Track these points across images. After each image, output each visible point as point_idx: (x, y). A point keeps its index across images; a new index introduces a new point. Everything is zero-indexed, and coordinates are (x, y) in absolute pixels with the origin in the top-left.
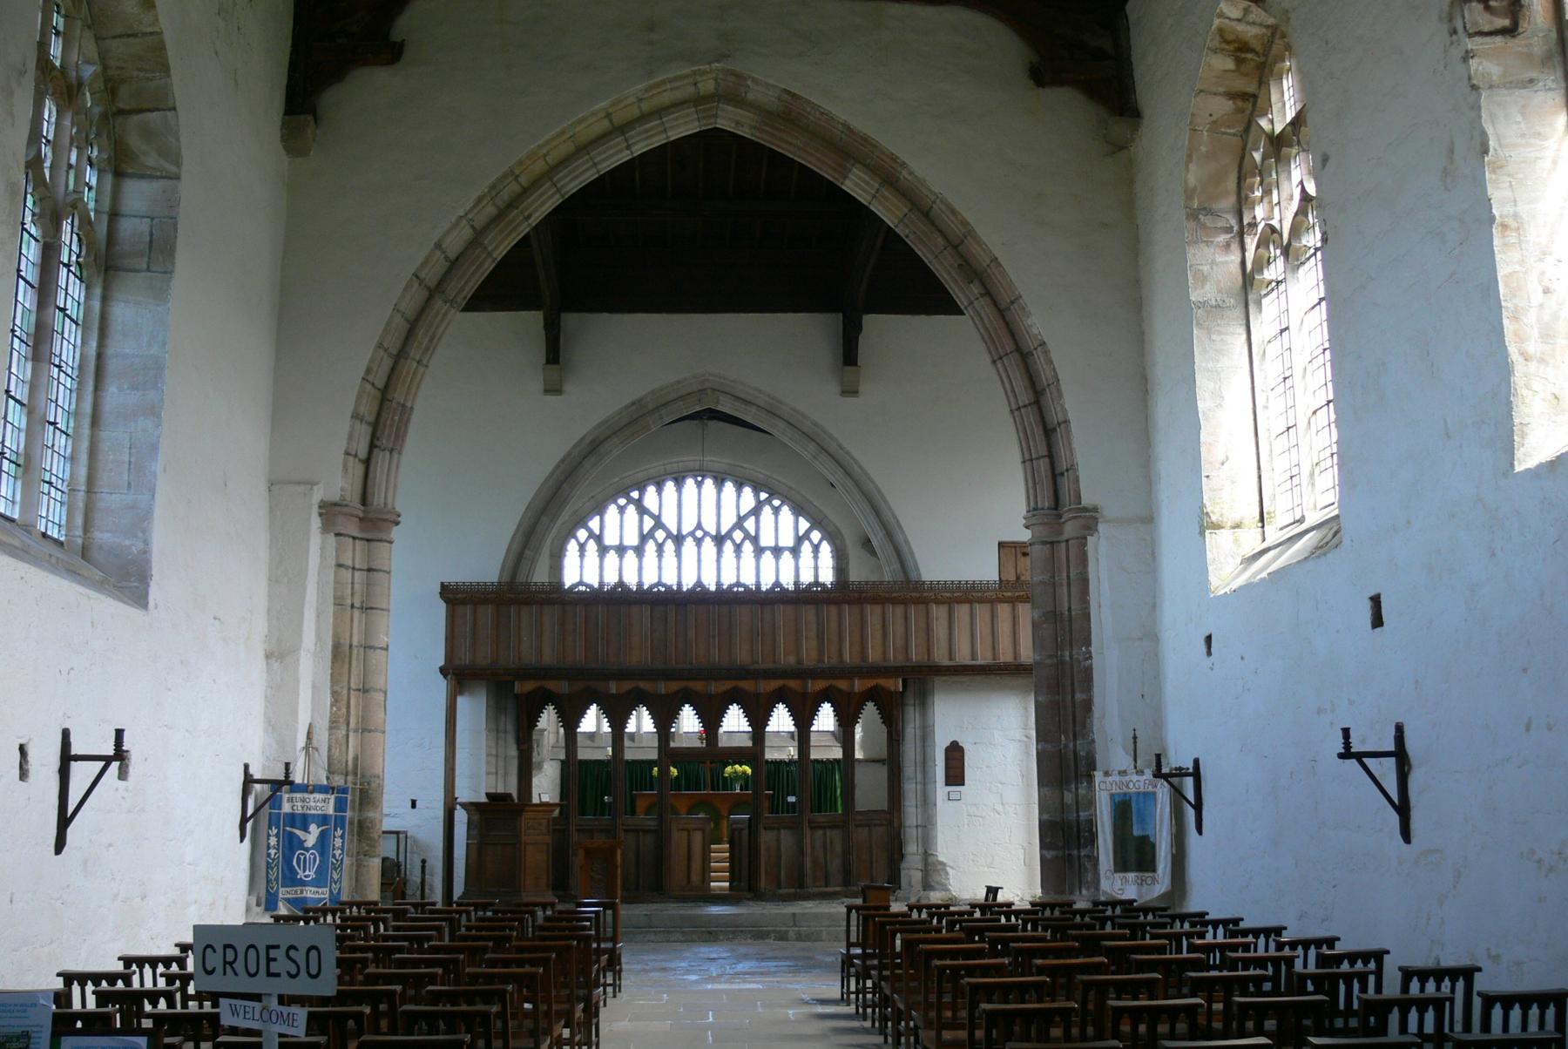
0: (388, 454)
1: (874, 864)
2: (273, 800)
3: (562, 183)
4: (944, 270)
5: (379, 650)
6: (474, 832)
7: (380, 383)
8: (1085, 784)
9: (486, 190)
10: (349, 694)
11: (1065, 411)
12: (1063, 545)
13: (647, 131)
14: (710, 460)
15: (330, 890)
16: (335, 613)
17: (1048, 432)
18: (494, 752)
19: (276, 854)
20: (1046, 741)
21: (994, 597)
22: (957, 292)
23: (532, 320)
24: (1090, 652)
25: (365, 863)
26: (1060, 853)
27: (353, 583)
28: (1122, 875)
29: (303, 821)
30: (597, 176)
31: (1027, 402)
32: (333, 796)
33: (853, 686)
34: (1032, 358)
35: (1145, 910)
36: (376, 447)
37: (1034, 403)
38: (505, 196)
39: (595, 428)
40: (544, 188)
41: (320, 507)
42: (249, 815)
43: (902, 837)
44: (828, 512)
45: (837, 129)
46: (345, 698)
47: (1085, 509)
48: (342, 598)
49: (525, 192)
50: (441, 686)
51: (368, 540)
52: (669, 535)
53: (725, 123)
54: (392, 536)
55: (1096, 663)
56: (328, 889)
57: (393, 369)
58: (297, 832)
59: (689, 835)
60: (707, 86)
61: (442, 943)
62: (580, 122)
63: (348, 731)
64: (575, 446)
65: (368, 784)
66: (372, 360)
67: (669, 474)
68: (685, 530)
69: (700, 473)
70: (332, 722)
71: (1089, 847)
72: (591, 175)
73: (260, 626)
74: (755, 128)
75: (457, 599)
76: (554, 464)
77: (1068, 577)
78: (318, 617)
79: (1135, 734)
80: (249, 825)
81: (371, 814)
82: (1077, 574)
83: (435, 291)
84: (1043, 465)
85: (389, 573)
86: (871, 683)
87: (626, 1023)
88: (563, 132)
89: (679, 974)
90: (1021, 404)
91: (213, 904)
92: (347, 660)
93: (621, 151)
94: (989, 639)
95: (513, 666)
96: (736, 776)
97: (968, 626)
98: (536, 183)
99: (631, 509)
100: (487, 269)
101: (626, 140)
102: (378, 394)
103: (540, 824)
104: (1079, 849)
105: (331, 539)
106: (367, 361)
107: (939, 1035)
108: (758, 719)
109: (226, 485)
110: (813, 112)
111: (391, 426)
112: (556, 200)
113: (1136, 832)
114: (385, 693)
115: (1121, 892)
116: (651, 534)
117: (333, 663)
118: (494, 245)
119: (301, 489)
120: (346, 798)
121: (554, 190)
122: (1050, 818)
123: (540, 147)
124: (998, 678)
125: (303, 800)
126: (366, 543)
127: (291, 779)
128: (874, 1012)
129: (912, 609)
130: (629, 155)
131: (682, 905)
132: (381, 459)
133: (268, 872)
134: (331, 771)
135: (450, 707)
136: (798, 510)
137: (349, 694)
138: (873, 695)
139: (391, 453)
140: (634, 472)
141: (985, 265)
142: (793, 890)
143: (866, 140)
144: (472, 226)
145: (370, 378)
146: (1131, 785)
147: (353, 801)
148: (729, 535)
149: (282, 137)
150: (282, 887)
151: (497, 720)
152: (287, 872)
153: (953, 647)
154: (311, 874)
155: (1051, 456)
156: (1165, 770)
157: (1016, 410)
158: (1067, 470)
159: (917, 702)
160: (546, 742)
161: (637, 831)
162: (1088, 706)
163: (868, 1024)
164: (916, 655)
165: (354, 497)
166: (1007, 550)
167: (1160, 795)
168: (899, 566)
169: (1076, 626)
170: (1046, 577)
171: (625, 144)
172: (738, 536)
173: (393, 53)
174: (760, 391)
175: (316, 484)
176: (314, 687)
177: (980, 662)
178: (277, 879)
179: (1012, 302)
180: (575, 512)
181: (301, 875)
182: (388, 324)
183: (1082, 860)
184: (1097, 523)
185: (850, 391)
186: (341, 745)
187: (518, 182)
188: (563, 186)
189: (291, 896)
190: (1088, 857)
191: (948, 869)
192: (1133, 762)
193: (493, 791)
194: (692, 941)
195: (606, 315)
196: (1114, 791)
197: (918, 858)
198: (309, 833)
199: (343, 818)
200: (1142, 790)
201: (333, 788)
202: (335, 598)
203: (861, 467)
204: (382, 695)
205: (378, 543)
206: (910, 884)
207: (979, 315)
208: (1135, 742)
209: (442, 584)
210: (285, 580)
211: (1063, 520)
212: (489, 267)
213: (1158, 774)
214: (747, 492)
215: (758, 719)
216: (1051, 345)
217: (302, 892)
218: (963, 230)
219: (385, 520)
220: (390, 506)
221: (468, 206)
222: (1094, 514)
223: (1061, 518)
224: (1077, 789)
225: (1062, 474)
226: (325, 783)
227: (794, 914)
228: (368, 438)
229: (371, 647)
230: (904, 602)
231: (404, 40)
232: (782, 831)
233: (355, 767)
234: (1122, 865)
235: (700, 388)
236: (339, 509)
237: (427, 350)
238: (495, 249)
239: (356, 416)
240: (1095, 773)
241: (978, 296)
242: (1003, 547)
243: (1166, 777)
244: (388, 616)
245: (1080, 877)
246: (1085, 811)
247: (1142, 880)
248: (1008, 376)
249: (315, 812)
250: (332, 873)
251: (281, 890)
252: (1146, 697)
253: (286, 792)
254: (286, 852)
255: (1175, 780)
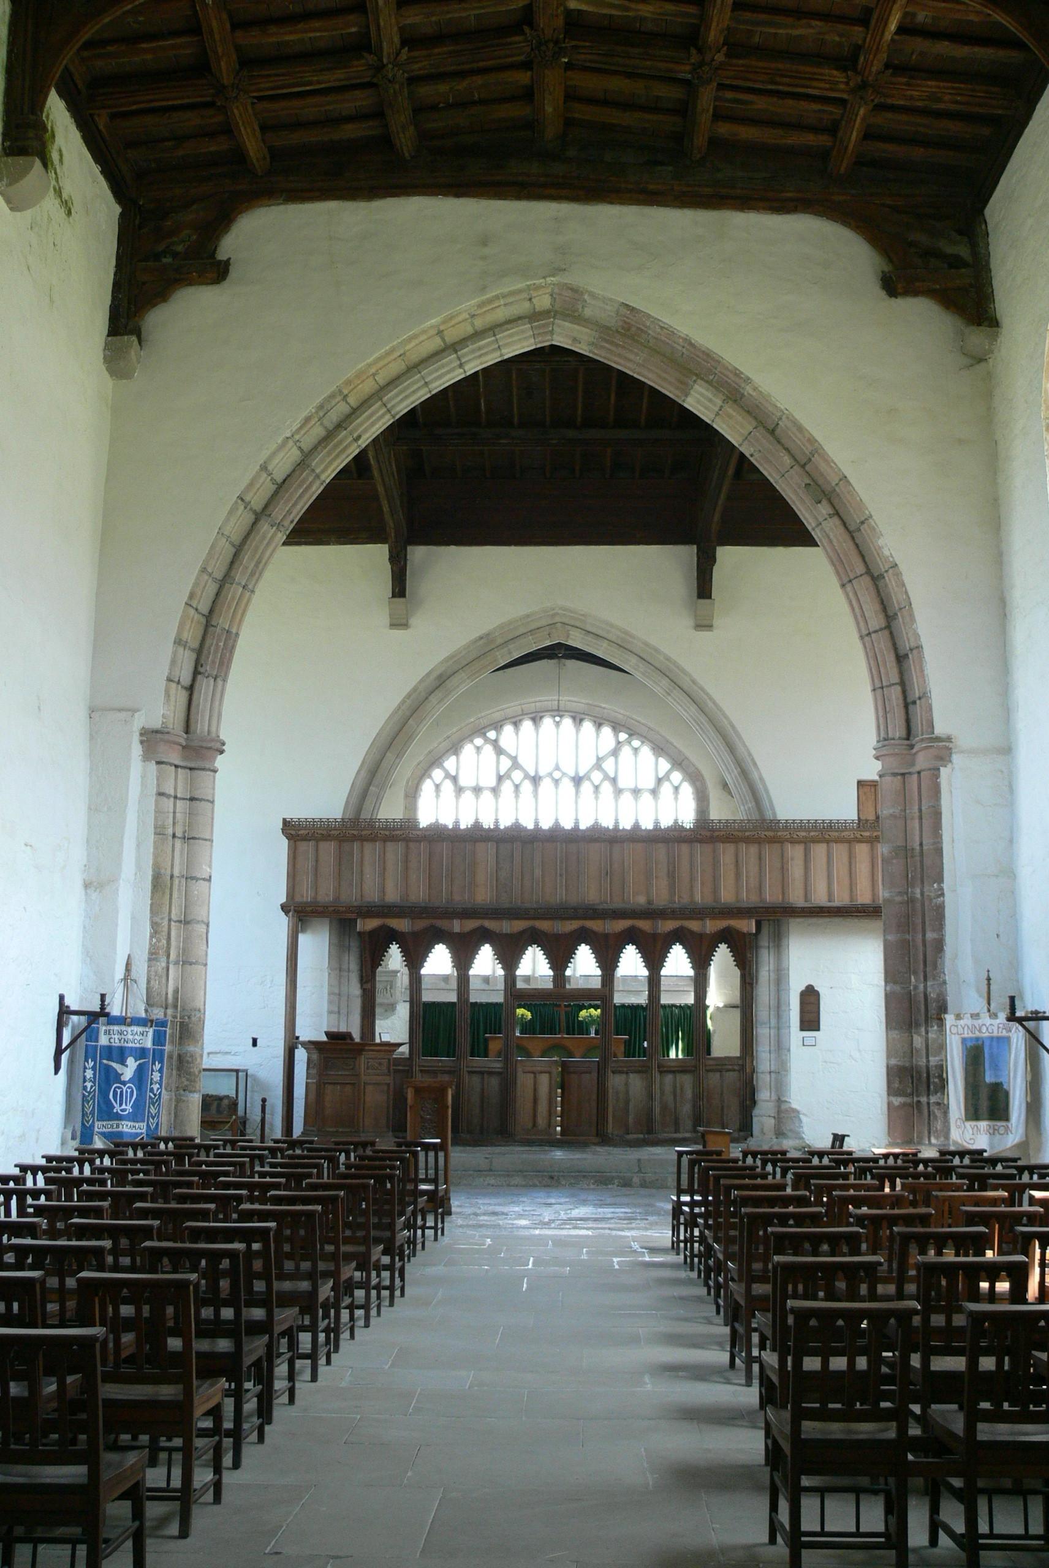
0: (212, 681)
1: (725, 1110)
2: (89, 1031)
3: (393, 403)
4: (809, 513)
5: (201, 881)
6: (313, 1071)
7: (204, 608)
8: (935, 1028)
9: (313, 411)
10: (169, 926)
11: (917, 636)
12: (916, 776)
13: (480, 348)
14: (567, 700)
15: (148, 1125)
16: (155, 842)
17: (901, 659)
18: (337, 991)
19: (92, 1087)
20: (895, 983)
21: (852, 836)
22: (804, 512)
23: (379, 552)
24: (942, 889)
25: (184, 1098)
26: (908, 1100)
27: (174, 812)
28: (973, 1123)
29: (120, 1054)
30: (429, 395)
31: (877, 628)
32: (151, 1030)
33: (704, 926)
34: (882, 581)
35: (993, 1161)
36: (200, 673)
37: (885, 628)
38: (334, 417)
39: (442, 663)
40: (373, 408)
41: (141, 734)
42: (64, 1045)
43: (755, 1083)
44: (687, 753)
45: (678, 344)
46: (166, 929)
47: (938, 739)
48: (164, 827)
49: (354, 412)
50: (282, 923)
51: (191, 769)
52: (527, 776)
53: (562, 340)
54: (216, 765)
55: (949, 899)
56: (145, 1124)
57: (218, 594)
58: (114, 1065)
59: (535, 1077)
60: (543, 302)
61: (321, 1181)
62: (410, 339)
63: (168, 963)
64: (422, 681)
65: (189, 1017)
66: (196, 584)
67: (527, 714)
68: (541, 773)
69: (558, 712)
70: (151, 953)
71: (939, 1094)
72: (423, 395)
73: (78, 854)
74: (593, 344)
75: (298, 835)
76: (400, 700)
77: (920, 810)
78: (138, 846)
79: (988, 976)
80: (64, 1057)
81: (191, 1048)
82: (929, 807)
83: (260, 515)
84: (896, 693)
85: (212, 802)
86: (721, 924)
87: (441, 1268)
88: (393, 350)
89: (511, 1219)
90: (871, 630)
91: (23, 1137)
92: (168, 891)
93: (453, 370)
94: (846, 882)
95: (355, 904)
96: (592, 1020)
97: (825, 866)
98: (365, 403)
99: (488, 749)
100: (314, 493)
101: (459, 358)
102: (203, 620)
103: (380, 1064)
104: (928, 1095)
105: (152, 766)
106: (191, 585)
107: (748, 1290)
108: (608, 961)
109: (39, 709)
110: (652, 327)
111: (216, 651)
112: (387, 421)
113: (989, 1078)
114: (208, 925)
115: (972, 1142)
116: (507, 775)
117: (152, 893)
118: (322, 467)
119: (123, 715)
120: (165, 1031)
121: (384, 410)
122: (899, 1063)
123: (369, 365)
124: (856, 920)
125: (121, 1033)
126: (188, 771)
127: (107, 1011)
128: (700, 1262)
129: (767, 848)
130: (461, 374)
131: (527, 1148)
132: (205, 686)
133: (83, 1105)
134: (150, 1003)
135: (292, 943)
136: (660, 749)
137: (169, 926)
138: (728, 937)
139: (215, 679)
140: (490, 712)
141: (834, 484)
142: (641, 1136)
143: (708, 355)
144: (300, 448)
145: (194, 604)
146: (984, 1029)
147: (172, 1035)
148: (587, 776)
149: (105, 358)
150: (98, 1120)
151: (340, 961)
152: (103, 1106)
153: (809, 888)
154: (128, 1108)
155: (903, 684)
156: (1019, 1013)
157: (866, 636)
158: (920, 698)
159: (771, 945)
160: (399, 984)
161: (482, 1073)
162: (939, 946)
163: (694, 1275)
164: (771, 896)
165: (177, 726)
166: (867, 789)
167: (1014, 1041)
168: (754, 803)
169: (927, 862)
170: (897, 811)
171: (458, 362)
172: (597, 776)
173: (218, 272)
174: (612, 626)
175: (138, 710)
176: (133, 918)
177: (836, 904)
178: (93, 1113)
179: (862, 523)
180: (430, 752)
181: (117, 1108)
182: (213, 547)
183: (932, 1108)
184: (951, 753)
185: (704, 625)
186: (160, 977)
187: (347, 402)
188: (393, 406)
189: (107, 1130)
190: (938, 1104)
191: (801, 1116)
192: (986, 1005)
193: (335, 1030)
194: (535, 1186)
195: (453, 547)
196: (966, 1035)
197: (771, 1105)
198: (127, 1066)
199: (162, 1052)
200: (995, 1034)
201: (152, 1021)
202: (156, 828)
203: (714, 703)
204: (205, 927)
205: (199, 772)
206: (763, 1132)
207: (828, 537)
208: (989, 985)
209: (284, 820)
210: (105, 809)
211: (914, 751)
212: (317, 489)
213: (1012, 1018)
214: (607, 731)
215: (608, 961)
216: (902, 567)
217: (118, 1126)
218: (810, 448)
219: (210, 748)
220: (214, 735)
221: (296, 426)
222: (947, 744)
223: (912, 749)
224: (927, 1033)
225: (914, 703)
226: (143, 1015)
227: (639, 1160)
228: (192, 664)
229: (192, 878)
230: (759, 841)
231: (230, 259)
232: (631, 1075)
233: (176, 999)
234: (973, 1113)
235: (550, 622)
236: (159, 736)
237: (252, 574)
238: (323, 471)
239: (179, 642)
240: (946, 1016)
241: (827, 517)
242: (862, 785)
243: (1020, 1021)
244: (212, 846)
245: (929, 1124)
246: (935, 1056)
247: (994, 1130)
248: (858, 600)
249: (133, 1045)
250: (149, 1107)
251: (96, 1124)
252: (1001, 936)
253: (103, 1024)
254: (103, 1086)
255: (1030, 1025)
